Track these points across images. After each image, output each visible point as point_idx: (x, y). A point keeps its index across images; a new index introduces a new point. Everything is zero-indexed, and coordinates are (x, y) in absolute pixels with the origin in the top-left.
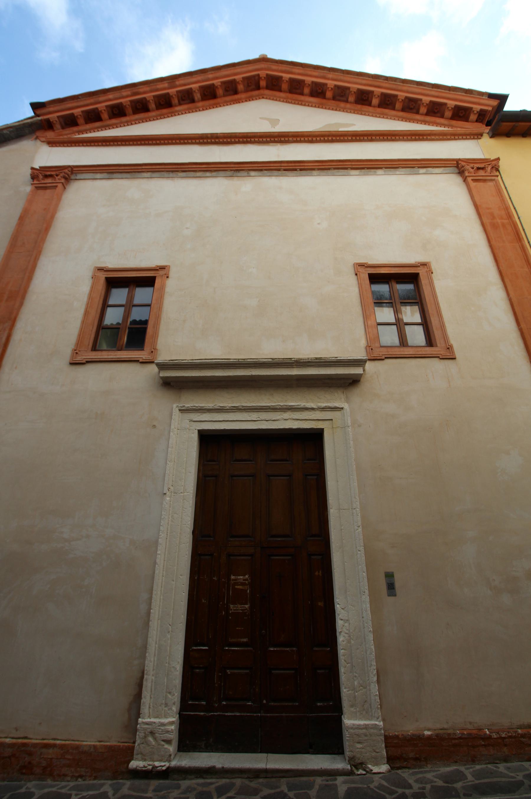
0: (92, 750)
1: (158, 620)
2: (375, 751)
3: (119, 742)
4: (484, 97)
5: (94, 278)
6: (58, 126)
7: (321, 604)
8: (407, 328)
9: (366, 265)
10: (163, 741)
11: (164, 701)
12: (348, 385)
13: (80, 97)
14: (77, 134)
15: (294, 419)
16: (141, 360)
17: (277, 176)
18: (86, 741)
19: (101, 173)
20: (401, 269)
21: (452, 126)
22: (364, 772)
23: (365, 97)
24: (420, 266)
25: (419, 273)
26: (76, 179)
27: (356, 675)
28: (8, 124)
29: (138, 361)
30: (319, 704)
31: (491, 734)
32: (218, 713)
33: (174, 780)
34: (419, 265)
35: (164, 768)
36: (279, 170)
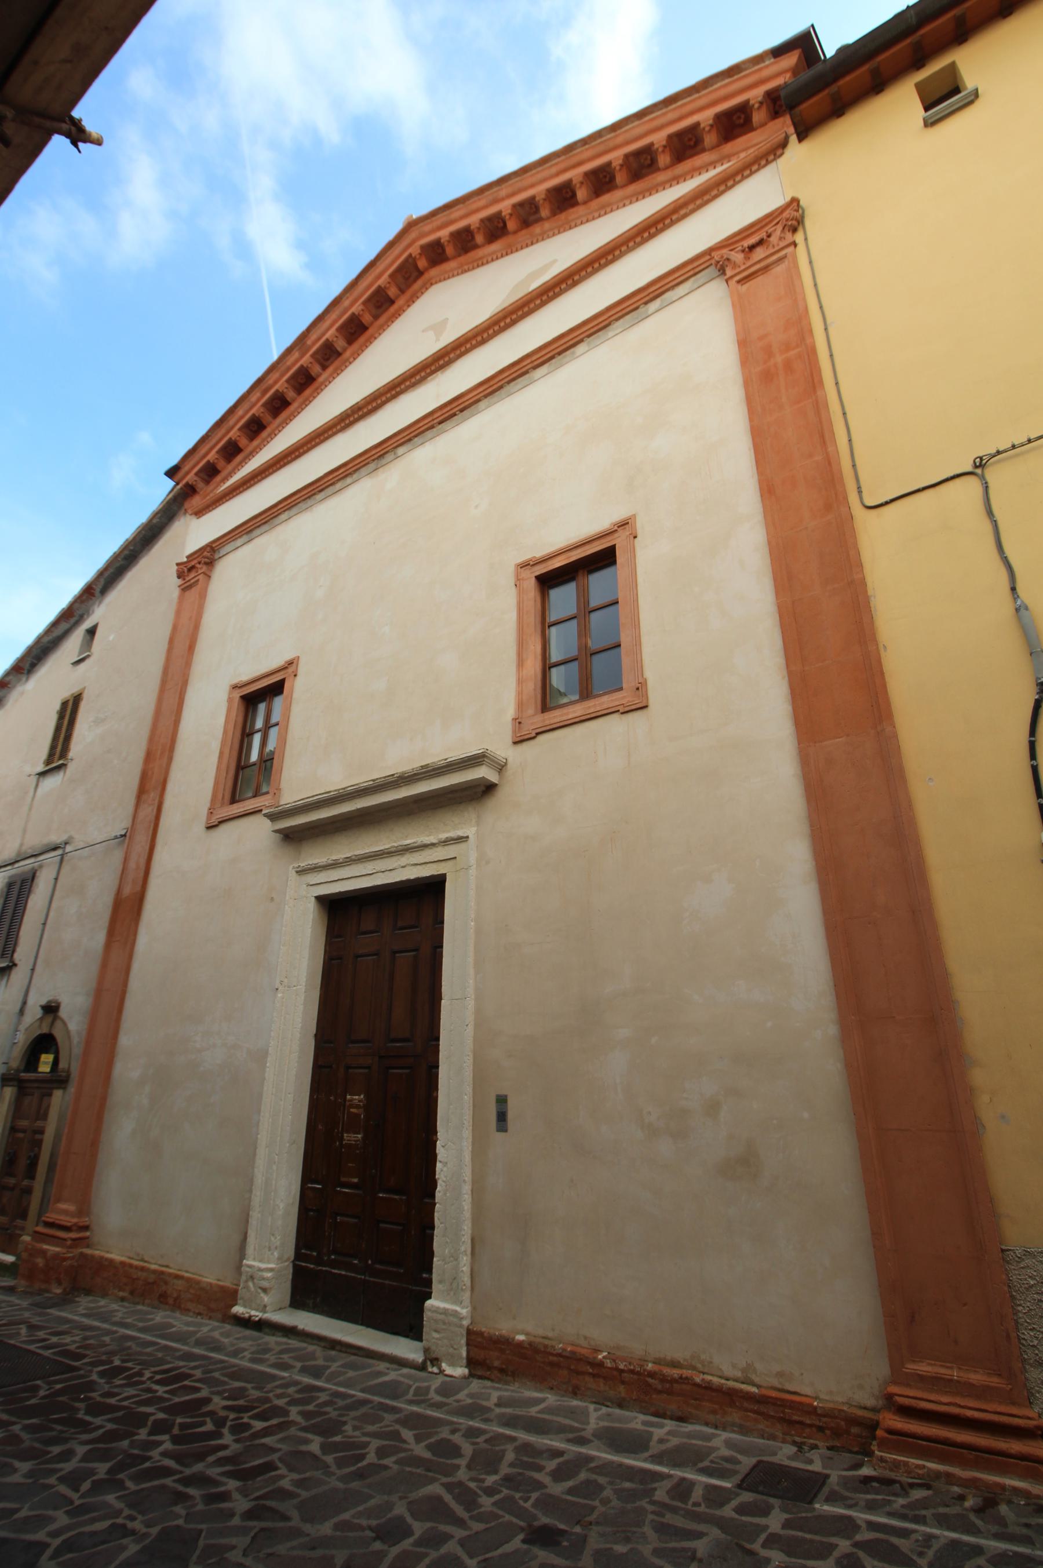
1: (266, 1147)
2: (452, 1347)
6: (200, 485)
9: (531, 563)
10: (261, 1288)
11: (267, 1244)
12: (482, 796)
13: (210, 434)
14: (222, 484)
17: (431, 439)
19: (240, 537)
21: (728, 157)
24: (616, 530)
26: (220, 558)
28: (154, 511)
31: (604, 1360)
36: (432, 427)
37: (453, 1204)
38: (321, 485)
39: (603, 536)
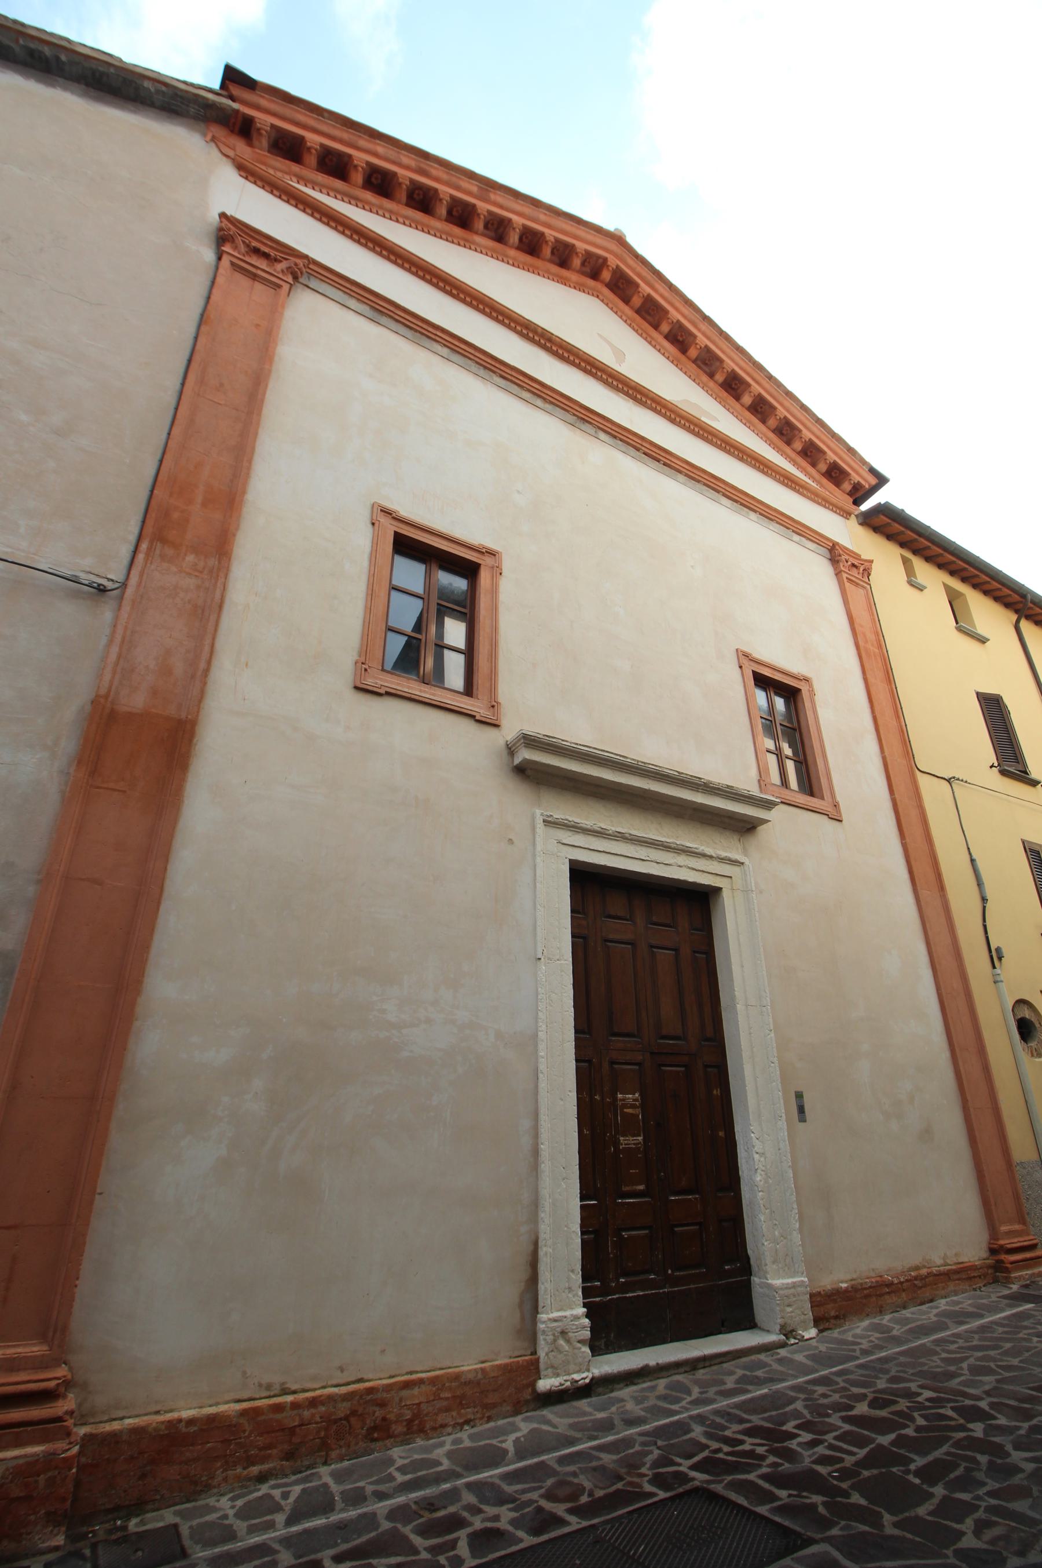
0: (480, 1376)
3: (510, 1357)
4: (864, 467)
5: (377, 525)
7: (721, 1134)
8: (446, 652)
9: (394, 515)
10: (579, 1342)
13: (326, 115)
14: (294, 179)
15: (689, 868)
16: (477, 718)
18: (463, 1366)
20: (784, 677)
21: (822, 486)
22: (797, 1341)
23: (736, 384)
25: (480, 564)
27: (777, 1223)
29: (473, 717)
30: (726, 1267)
32: (617, 1296)
33: (599, 1395)
34: (484, 550)
35: (587, 1381)
36: (638, 449)
37: (776, 1189)
38: (594, 420)
39: (413, 525)
